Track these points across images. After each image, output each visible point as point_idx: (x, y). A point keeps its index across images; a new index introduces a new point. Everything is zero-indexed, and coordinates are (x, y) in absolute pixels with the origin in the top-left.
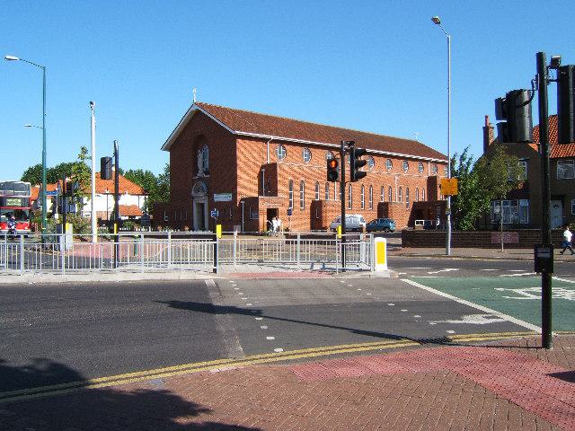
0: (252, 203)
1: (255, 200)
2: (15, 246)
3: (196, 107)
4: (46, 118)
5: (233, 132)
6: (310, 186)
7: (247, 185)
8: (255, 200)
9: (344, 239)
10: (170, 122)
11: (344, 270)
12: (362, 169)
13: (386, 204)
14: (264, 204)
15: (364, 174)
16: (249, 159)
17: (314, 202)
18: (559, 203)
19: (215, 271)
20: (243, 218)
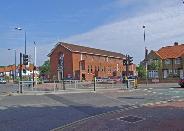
0: (78, 72)
1: (79, 71)
2: (153, 76)
3: (59, 44)
4: (26, 42)
5: (72, 51)
6: (94, 66)
7: (76, 67)
8: (79, 71)
9: (127, 81)
10: (51, 47)
11: (127, 89)
12: (132, 62)
13: (115, 72)
14: (82, 72)
15: (132, 63)
16: (76, 59)
17: (113, 72)
18: (166, 71)
19: (94, 90)
20: (77, 76)
